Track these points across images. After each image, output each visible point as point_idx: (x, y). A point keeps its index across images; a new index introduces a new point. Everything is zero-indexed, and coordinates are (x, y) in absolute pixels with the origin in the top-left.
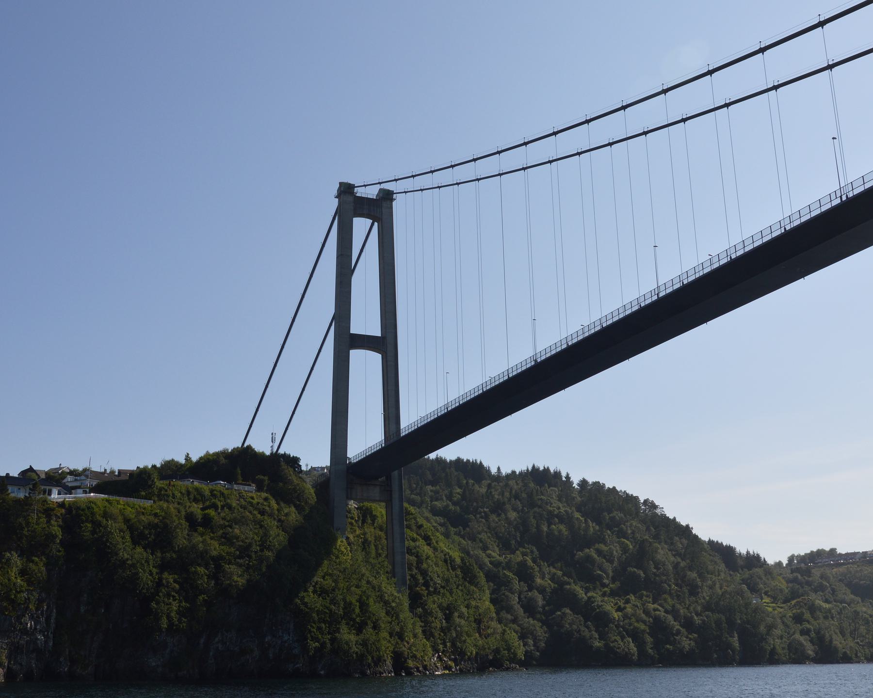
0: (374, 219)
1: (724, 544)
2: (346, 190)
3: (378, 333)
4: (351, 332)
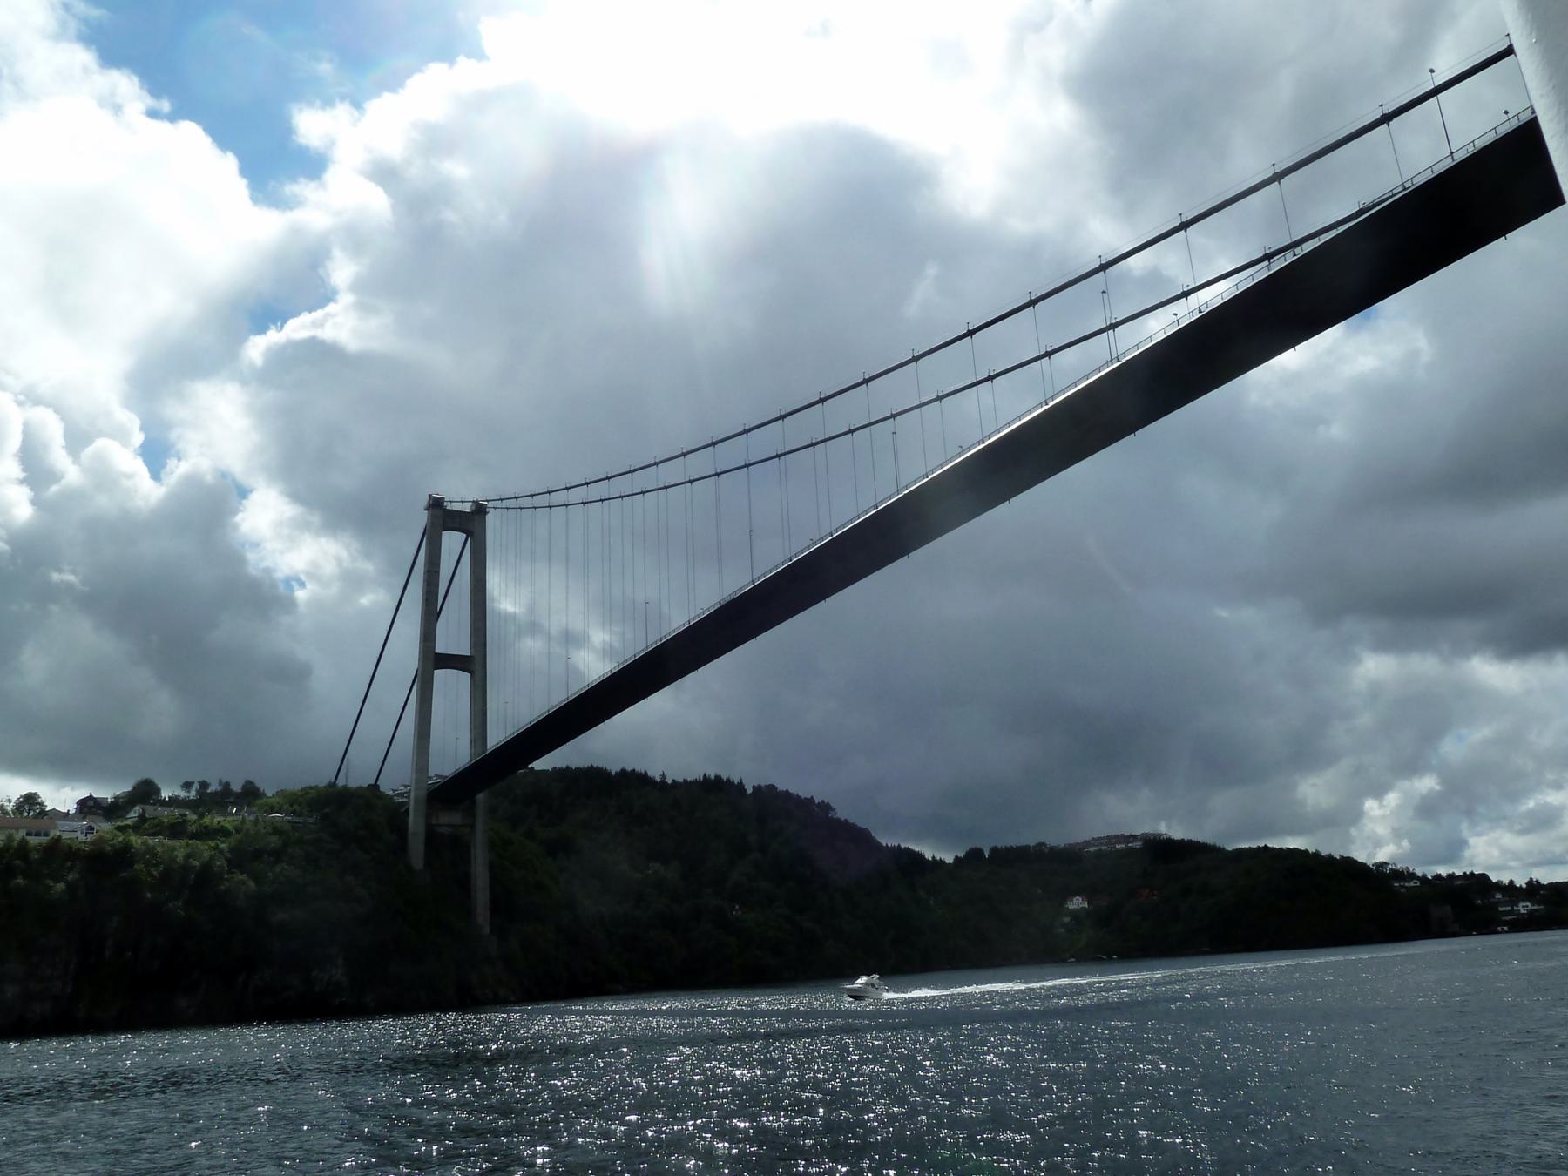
0: (469, 533)
1: (1186, 839)
2: (436, 504)
3: (467, 653)
4: (436, 652)
